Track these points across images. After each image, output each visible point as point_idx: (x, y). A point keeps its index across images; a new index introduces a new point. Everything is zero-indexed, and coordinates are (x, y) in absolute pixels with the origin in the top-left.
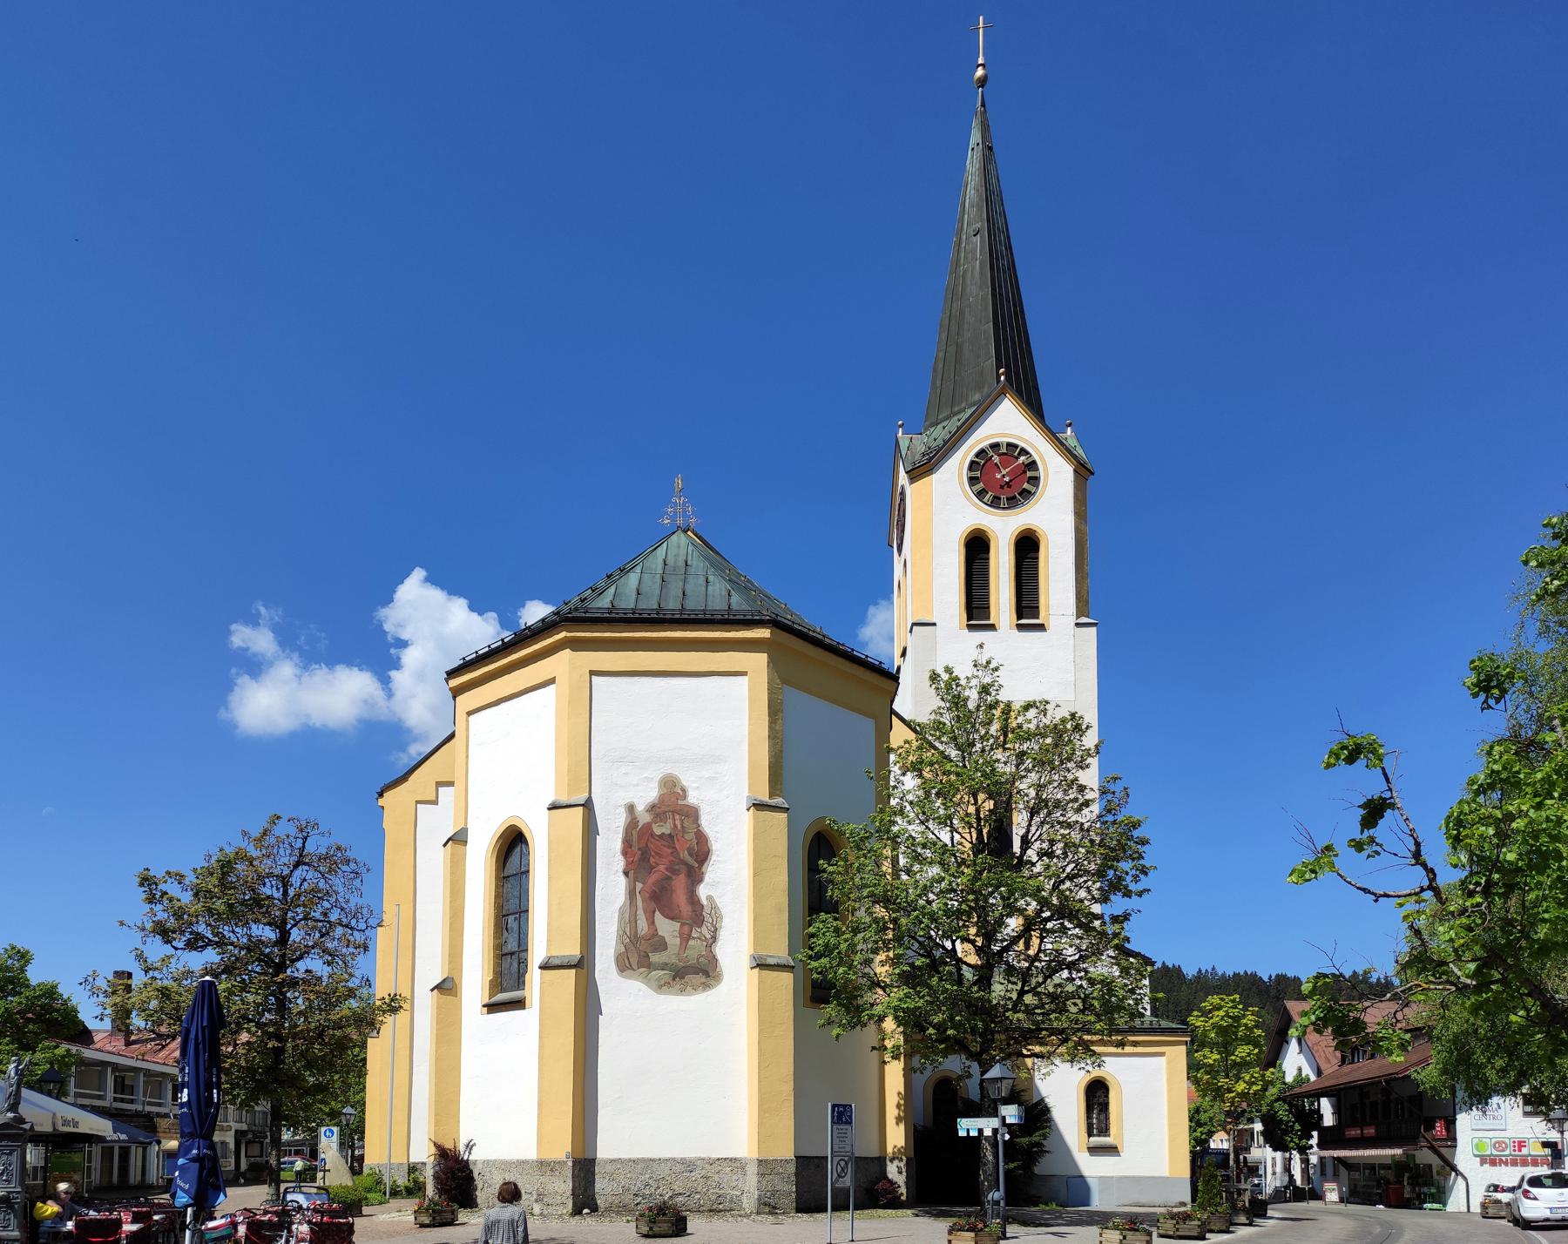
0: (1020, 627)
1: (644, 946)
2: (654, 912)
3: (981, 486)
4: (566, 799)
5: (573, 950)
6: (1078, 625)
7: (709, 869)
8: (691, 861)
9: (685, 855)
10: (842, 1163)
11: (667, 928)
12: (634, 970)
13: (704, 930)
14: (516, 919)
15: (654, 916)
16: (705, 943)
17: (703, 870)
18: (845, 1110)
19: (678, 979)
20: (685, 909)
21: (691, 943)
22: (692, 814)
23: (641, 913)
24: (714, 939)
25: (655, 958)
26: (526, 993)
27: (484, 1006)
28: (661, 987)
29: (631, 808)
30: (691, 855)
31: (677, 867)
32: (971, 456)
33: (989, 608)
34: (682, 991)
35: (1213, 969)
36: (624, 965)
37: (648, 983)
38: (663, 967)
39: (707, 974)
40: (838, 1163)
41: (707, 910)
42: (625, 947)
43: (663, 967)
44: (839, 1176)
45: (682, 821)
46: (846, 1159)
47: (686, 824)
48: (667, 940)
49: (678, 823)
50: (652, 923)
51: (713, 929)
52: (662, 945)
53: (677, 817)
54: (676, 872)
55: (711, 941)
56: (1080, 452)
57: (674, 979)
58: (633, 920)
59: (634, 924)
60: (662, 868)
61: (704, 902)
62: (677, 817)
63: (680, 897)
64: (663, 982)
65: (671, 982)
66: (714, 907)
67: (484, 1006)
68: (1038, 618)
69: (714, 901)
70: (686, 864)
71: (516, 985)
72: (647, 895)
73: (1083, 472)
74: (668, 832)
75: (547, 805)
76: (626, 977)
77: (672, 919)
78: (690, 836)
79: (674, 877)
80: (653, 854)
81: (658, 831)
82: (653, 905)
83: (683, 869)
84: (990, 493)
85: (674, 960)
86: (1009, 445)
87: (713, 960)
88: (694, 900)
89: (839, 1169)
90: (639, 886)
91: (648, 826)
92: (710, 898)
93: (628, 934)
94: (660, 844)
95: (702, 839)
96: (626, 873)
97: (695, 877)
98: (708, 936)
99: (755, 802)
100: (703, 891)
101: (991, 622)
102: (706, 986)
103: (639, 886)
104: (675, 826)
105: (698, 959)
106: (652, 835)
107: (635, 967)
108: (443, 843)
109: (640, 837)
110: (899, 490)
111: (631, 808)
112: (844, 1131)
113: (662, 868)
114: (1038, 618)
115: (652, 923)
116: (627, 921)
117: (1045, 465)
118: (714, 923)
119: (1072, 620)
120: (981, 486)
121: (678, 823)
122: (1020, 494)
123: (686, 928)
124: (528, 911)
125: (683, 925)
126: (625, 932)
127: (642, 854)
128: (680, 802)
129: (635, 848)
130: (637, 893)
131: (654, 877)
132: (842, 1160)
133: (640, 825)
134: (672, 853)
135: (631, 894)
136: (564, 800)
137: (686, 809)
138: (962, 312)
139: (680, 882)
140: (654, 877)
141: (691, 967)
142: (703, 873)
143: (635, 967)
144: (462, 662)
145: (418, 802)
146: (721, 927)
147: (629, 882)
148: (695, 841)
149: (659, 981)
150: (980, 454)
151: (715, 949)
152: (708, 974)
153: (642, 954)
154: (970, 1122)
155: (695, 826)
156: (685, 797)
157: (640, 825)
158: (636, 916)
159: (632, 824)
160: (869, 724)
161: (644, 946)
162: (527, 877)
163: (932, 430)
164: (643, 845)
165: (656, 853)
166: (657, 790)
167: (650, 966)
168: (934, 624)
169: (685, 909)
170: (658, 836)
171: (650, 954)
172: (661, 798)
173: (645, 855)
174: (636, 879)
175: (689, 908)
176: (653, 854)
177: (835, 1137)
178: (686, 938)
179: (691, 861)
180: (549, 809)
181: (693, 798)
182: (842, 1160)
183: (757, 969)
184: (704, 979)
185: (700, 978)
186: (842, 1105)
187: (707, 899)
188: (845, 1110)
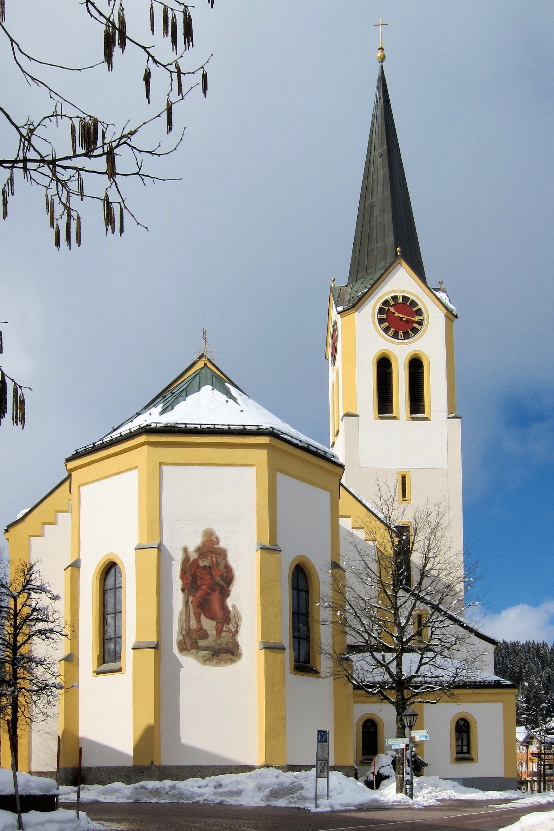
0: (413, 419)
1: (194, 636)
2: (200, 615)
3: (386, 324)
4: (146, 543)
5: (153, 638)
6: (449, 418)
7: (233, 589)
8: (222, 583)
9: (218, 579)
10: (323, 764)
11: (209, 625)
12: (188, 651)
13: (231, 627)
14: (112, 617)
15: (200, 618)
16: (231, 635)
17: (230, 589)
18: (324, 734)
19: (215, 657)
20: (219, 613)
21: (223, 634)
22: (223, 553)
23: (192, 616)
24: (237, 632)
25: (201, 643)
26: (122, 664)
27: (94, 672)
28: (206, 661)
29: (185, 550)
30: (222, 579)
31: (214, 587)
32: (379, 305)
33: (393, 405)
34: (218, 664)
35: (533, 641)
36: (183, 648)
37: (197, 657)
38: (206, 648)
39: (233, 653)
40: (321, 764)
41: (232, 614)
42: (183, 636)
43: (206, 648)
44: (321, 772)
45: (216, 558)
46: (324, 762)
47: (219, 560)
48: (208, 632)
49: (214, 559)
50: (199, 621)
51: (236, 626)
52: (204, 635)
53: (214, 555)
54: (214, 590)
55: (235, 633)
56: (451, 306)
57: (213, 656)
58: (188, 620)
59: (188, 623)
60: (204, 587)
61: (230, 608)
62: (214, 555)
63: (216, 606)
64: (206, 658)
65: (211, 658)
66: (236, 612)
67: (94, 672)
68: (424, 413)
69: (236, 608)
70: (219, 585)
71: (114, 659)
72: (196, 604)
73: (451, 316)
74: (208, 564)
75: (134, 547)
76: (184, 655)
77: (211, 619)
78: (222, 567)
79: (212, 593)
80: (199, 578)
81: (202, 564)
82: (200, 610)
83: (218, 588)
84: (392, 329)
85: (213, 645)
86: (404, 298)
87: (236, 645)
88: (224, 608)
89: (321, 768)
90: (191, 598)
91: (196, 561)
92: (234, 606)
93: (185, 628)
94: (203, 572)
95: (228, 569)
96: (183, 590)
97: (225, 593)
98: (233, 630)
99: (262, 547)
100: (230, 602)
101: (394, 415)
102: (232, 661)
103: (191, 598)
104: (212, 561)
105: (227, 644)
106: (198, 566)
107: (189, 648)
108: (64, 569)
109: (191, 568)
110: (333, 323)
111: (185, 550)
112: (324, 746)
113: (204, 587)
114: (424, 413)
115: (199, 621)
116: (184, 620)
117: (427, 311)
118: (237, 622)
119: (446, 414)
120: (386, 324)
121: (214, 559)
122: (411, 330)
123: (220, 626)
124: (121, 612)
125: (218, 623)
126: (183, 627)
127: (193, 578)
128: (215, 546)
129: (188, 575)
130: (190, 603)
131: (199, 593)
132: (323, 762)
133: (191, 560)
134: (211, 578)
135: (186, 603)
136: (145, 543)
137: (218, 550)
138: (372, 206)
139: (215, 596)
140: (199, 593)
141: (223, 649)
142: (229, 591)
143: (189, 648)
144: (75, 452)
145: (30, 536)
146: (241, 624)
147: (185, 596)
148: (224, 571)
149: (204, 658)
150: (386, 303)
151: (237, 638)
152: (234, 653)
153: (194, 641)
154: (393, 740)
155: (224, 561)
156: (218, 542)
157: (191, 560)
158: (189, 618)
159: (186, 560)
160: (326, 496)
161: (194, 636)
162: (456, 737)
163: (354, 284)
164: (193, 572)
165: (202, 578)
166: (201, 538)
167: (198, 648)
168: (357, 416)
169: (219, 613)
170: (202, 567)
171: (198, 641)
172: (204, 544)
173: (194, 577)
174: (189, 594)
175: (222, 612)
176: (199, 578)
177: (319, 749)
178: (219, 631)
179: (222, 583)
180: (136, 549)
181: (222, 544)
182: (323, 762)
183: (264, 650)
184: (231, 657)
185: (229, 656)
186: (322, 731)
187: (232, 607)
188: (324, 734)
